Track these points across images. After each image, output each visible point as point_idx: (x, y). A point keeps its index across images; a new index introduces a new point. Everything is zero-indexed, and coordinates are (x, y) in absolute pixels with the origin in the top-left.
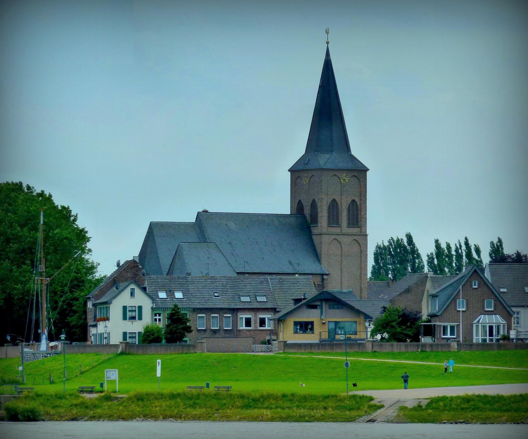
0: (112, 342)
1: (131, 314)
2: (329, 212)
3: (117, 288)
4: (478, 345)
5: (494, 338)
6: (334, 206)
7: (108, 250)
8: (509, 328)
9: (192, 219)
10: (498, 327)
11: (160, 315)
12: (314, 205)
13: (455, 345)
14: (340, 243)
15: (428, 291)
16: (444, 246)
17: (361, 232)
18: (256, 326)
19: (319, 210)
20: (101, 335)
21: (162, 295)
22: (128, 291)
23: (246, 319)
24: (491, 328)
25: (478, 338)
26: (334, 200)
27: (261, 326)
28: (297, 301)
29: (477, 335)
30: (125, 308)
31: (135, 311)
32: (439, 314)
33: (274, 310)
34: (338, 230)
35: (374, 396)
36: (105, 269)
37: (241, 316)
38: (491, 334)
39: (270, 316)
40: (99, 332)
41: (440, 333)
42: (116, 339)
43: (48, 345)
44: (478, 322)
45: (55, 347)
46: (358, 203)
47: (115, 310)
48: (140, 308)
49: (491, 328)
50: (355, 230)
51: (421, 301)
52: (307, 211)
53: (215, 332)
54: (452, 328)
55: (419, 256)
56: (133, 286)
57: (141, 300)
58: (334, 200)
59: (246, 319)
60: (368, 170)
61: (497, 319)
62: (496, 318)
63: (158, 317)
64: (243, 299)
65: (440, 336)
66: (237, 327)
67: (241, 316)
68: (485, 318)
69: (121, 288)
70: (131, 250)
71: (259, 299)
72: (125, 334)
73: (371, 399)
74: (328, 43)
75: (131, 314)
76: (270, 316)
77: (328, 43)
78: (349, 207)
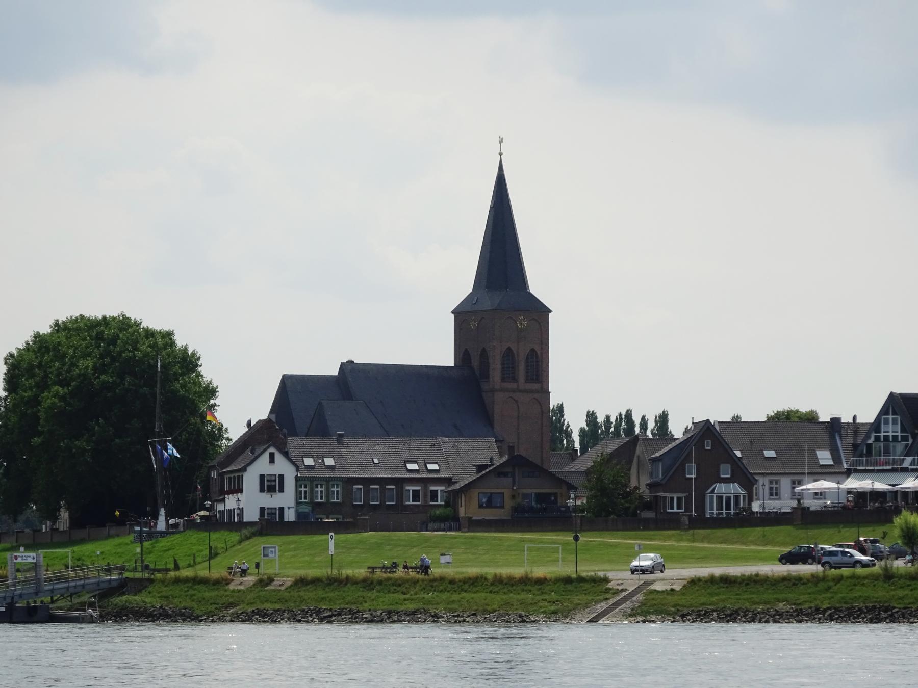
0: (246, 519)
1: (270, 485)
2: (503, 364)
3: (252, 453)
4: (712, 518)
5: (732, 511)
6: (509, 354)
7: (240, 406)
8: (751, 500)
9: (335, 372)
10: (737, 498)
11: (305, 487)
12: (484, 355)
13: (685, 520)
14: (517, 401)
15: (639, 457)
16: (601, 419)
17: (542, 388)
18: (426, 501)
19: (491, 361)
20: (231, 512)
21: (309, 461)
22: (266, 457)
23: (413, 491)
24: (729, 499)
25: (711, 511)
26: (509, 349)
27: (432, 500)
28: (480, 468)
29: (711, 509)
30: (262, 477)
31: (275, 481)
32: (663, 482)
33: (448, 481)
34: (514, 386)
35: (610, 575)
36: (235, 431)
37: (408, 488)
38: (728, 508)
39: (443, 488)
40: (227, 508)
41: (664, 506)
42: (252, 515)
43: (167, 521)
44: (713, 491)
45: (176, 526)
46: (539, 352)
47: (250, 480)
48: (282, 477)
49: (729, 499)
50: (536, 386)
51: (629, 470)
52: (475, 363)
53: (375, 507)
54: (679, 499)
55: (568, 434)
56: (272, 450)
57: (282, 467)
58: (509, 349)
59: (413, 491)
60: (551, 311)
61: (734, 489)
62: (735, 488)
63: (303, 489)
64: (411, 466)
65: (665, 510)
66: (402, 501)
67: (408, 488)
68: (720, 488)
69: (257, 453)
70: (261, 411)
71: (430, 467)
72: (262, 510)
73: (606, 580)
74: (501, 154)
75: (270, 485)
76: (443, 488)
77: (501, 154)
78: (527, 357)
